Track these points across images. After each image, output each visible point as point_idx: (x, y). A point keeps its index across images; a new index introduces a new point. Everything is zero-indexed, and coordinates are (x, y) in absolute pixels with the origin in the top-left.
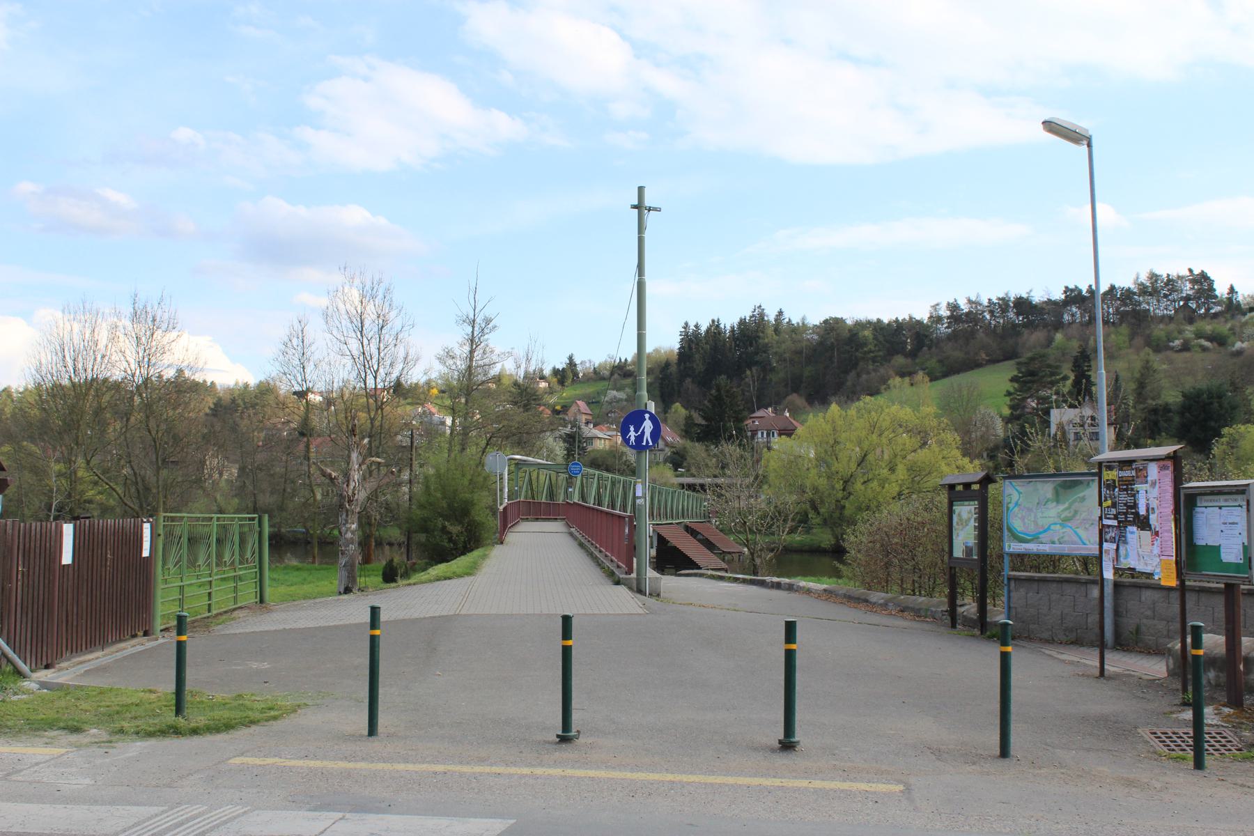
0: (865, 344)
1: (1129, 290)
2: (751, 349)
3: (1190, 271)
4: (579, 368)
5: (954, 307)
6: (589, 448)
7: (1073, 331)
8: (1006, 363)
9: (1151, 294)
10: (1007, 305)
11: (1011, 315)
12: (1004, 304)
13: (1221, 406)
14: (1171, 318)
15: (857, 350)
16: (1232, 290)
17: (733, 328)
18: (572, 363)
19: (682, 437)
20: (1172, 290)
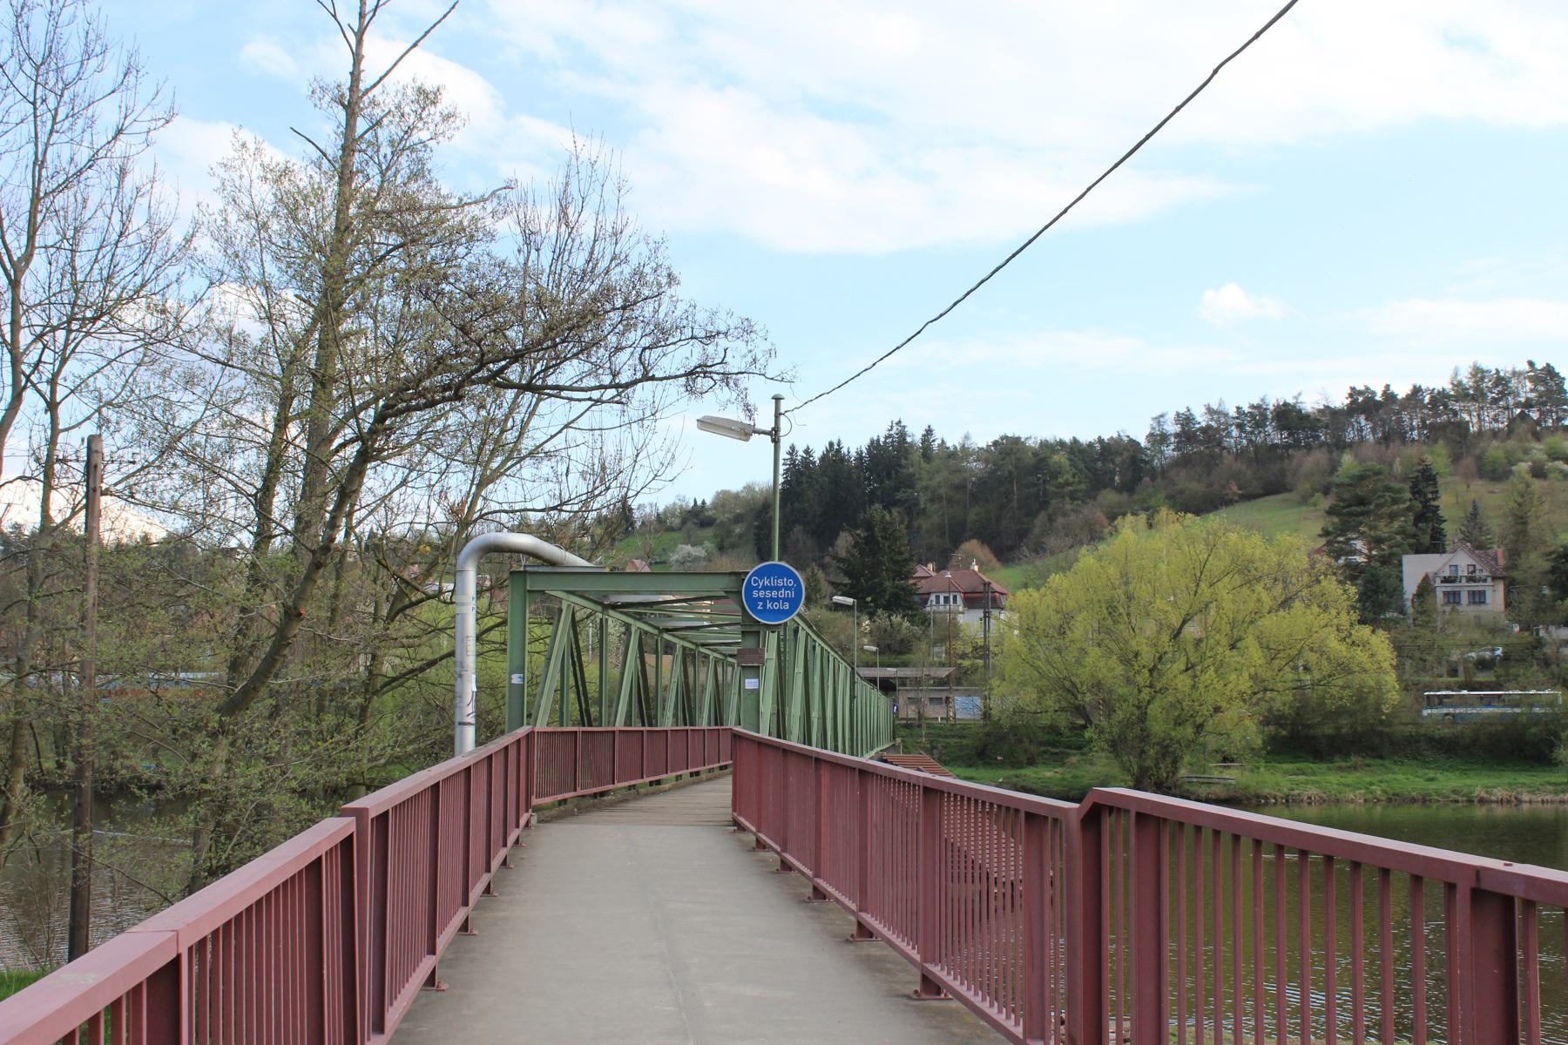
0: (1055, 474)
3: (1531, 364)
9: (1474, 398)
10: (1264, 417)
12: (1257, 417)
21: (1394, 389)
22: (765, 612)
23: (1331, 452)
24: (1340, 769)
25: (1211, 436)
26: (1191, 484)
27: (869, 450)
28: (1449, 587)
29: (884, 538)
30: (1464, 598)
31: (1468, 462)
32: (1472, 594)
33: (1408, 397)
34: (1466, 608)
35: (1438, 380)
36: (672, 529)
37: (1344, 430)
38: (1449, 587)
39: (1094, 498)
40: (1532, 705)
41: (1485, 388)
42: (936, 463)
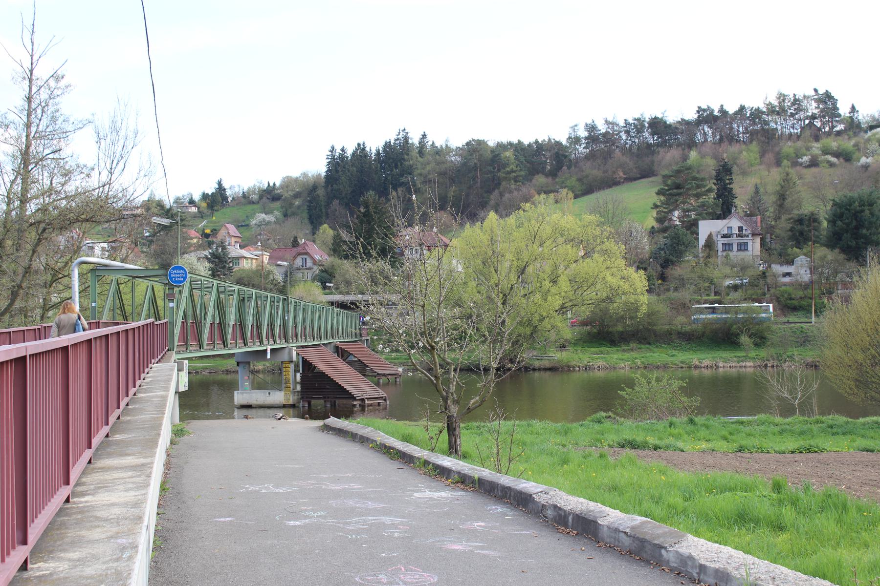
0: (505, 165)
1: (758, 110)
2: (396, 171)
3: (816, 90)
5: (591, 128)
6: (236, 268)
7: (707, 149)
8: (645, 181)
9: (778, 114)
10: (643, 126)
11: (646, 134)
12: (639, 126)
13: (872, 214)
14: (798, 137)
15: (499, 170)
16: (853, 109)
17: (378, 151)
18: (221, 189)
19: (329, 255)
20: (799, 110)
22: (175, 282)
23: (683, 150)
24: (624, 350)
25: (609, 138)
26: (593, 171)
27: (384, 150)
29: (375, 213)
30: (735, 247)
31: (770, 157)
32: (739, 244)
33: (736, 113)
34: (735, 254)
35: (756, 101)
36: (253, 203)
37: (695, 134)
38: (726, 240)
39: (531, 181)
40: (737, 313)
42: (427, 158)
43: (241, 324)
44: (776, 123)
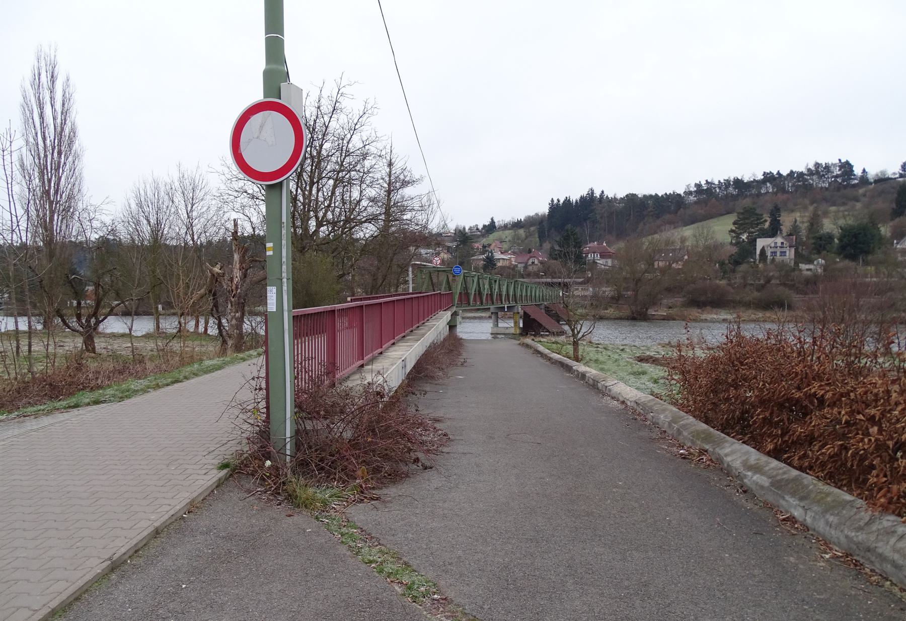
4: (497, 224)
12: (727, 183)
16: (864, 171)
18: (493, 222)
21: (781, 172)
28: (773, 250)
30: (778, 254)
32: (781, 252)
33: (788, 175)
35: (800, 168)
41: (820, 170)
43: (508, 295)
44: (814, 180)
